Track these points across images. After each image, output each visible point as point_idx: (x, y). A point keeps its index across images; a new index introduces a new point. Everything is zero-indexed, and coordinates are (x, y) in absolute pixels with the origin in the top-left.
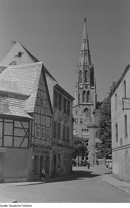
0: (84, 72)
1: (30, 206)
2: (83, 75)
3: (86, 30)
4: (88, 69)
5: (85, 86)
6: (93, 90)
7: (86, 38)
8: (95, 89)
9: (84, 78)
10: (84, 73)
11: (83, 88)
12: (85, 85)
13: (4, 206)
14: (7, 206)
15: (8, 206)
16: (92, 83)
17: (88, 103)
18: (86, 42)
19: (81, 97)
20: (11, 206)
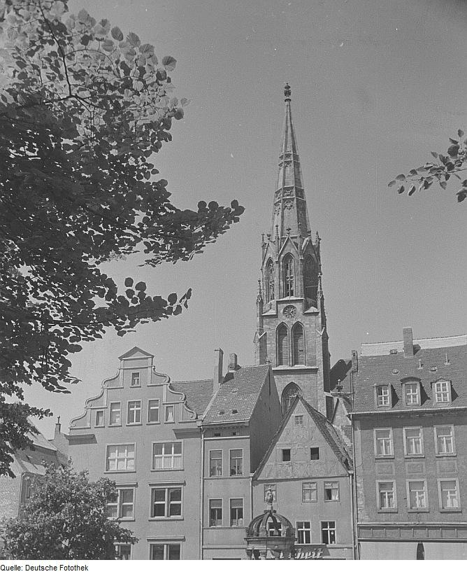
0: (281, 259)
1: (84, 568)
2: (277, 270)
3: (289, 124)
4: (293, 251)
5: (286, 308)
6: (313, 318)
7: (290, 149)
8: (320, 314)
9: (282, 283)
10: (281, 263)
11: (276, 316)
12: (285, 305)
13: (12, 567)
14: (18, 568)
15: (24, 568)
16: (311, 293)
17: (297, 367)
18: (288, 163)
19: (271, 346)
20: (32, 568)
